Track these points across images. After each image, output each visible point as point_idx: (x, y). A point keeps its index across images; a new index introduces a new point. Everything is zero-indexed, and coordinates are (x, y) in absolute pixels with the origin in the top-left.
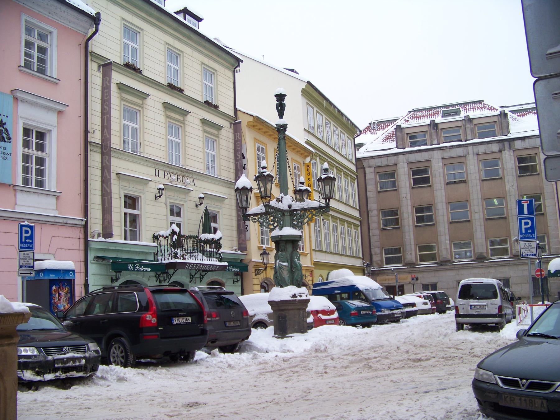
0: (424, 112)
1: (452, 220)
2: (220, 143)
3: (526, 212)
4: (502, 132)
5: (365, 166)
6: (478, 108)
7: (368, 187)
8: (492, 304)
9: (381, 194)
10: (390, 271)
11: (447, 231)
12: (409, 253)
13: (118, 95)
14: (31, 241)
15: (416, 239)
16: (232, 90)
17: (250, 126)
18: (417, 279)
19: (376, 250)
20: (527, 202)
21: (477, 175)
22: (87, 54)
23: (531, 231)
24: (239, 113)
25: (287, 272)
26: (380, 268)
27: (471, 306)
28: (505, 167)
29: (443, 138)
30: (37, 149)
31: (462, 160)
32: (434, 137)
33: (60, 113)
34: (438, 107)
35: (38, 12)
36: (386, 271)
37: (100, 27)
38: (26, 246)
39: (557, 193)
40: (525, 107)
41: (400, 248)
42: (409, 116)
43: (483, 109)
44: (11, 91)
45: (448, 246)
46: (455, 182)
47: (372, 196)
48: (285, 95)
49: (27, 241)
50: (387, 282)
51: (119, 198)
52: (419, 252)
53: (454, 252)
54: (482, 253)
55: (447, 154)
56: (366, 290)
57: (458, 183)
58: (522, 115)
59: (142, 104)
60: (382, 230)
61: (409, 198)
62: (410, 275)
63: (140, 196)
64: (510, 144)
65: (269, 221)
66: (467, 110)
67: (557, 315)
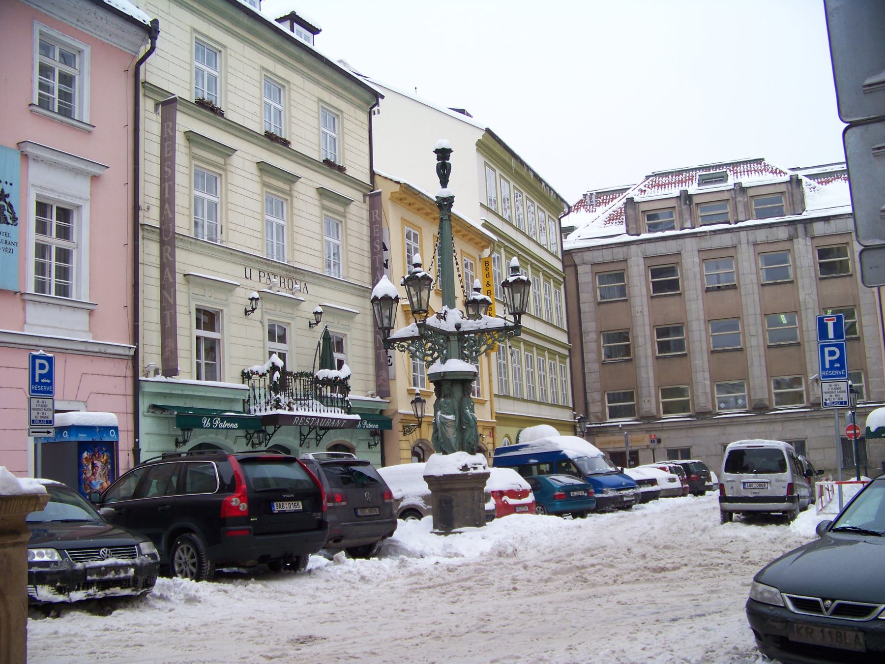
0: (670, 176)
1: (714, 347)
2: (348, 227)
3: (831, 335)
4: (794, 209)
5: (577, 262)
6: (755, 170)
7: (581, 295)
8: (777, 481)
9: (603, 307)
10: (617, 429)
11: (706, 365)
12: (646, 401)
13: (187, 151)
14: (49, 381)
15: (657, 378)
16: (367, 142)
17: (395, 199)
18: (659, 441)
19: (594, 396)
20: (833, 320)
21: (753, 277)
22: (138, 85)
23: (839, 365)
24: (377, 178)
25: (454, 430)
26: (600, 424)
27: (744, 483)
28: (798, 263)
29: (700, 219)
30: (59, 235)
31: (731, 252)
32: (686, 216)
33: (95, 178)
34: (692, 170)
35: (60, 19)
36: (609, 429)
37: (158, 42)
38: (41, 388)
39: (881, 306)
40: (829, 169)
41: (632, 392)
42: (646, 183)
43: (764, 172)
44: (18, 144)
45: (708, 390)
46: (719, 287)
47: (587, 310)
48: (450, 151)
49: (43, 381)
50: (611, 446)
51: (188, 313)
52: (662, 398)
53: (718, 398)
54: (761, 400)
55: (706, 244)
56: (578, 458)
57: (724, 290)
58: (825, 182)
59: (225, 165)
60: (603, 364)
61: (646, 312)
62: (648, 435)
63: (222, 310)
64: (805, 228)
65: (425, 349)
66: (739, 174)
67: (880, 498)
